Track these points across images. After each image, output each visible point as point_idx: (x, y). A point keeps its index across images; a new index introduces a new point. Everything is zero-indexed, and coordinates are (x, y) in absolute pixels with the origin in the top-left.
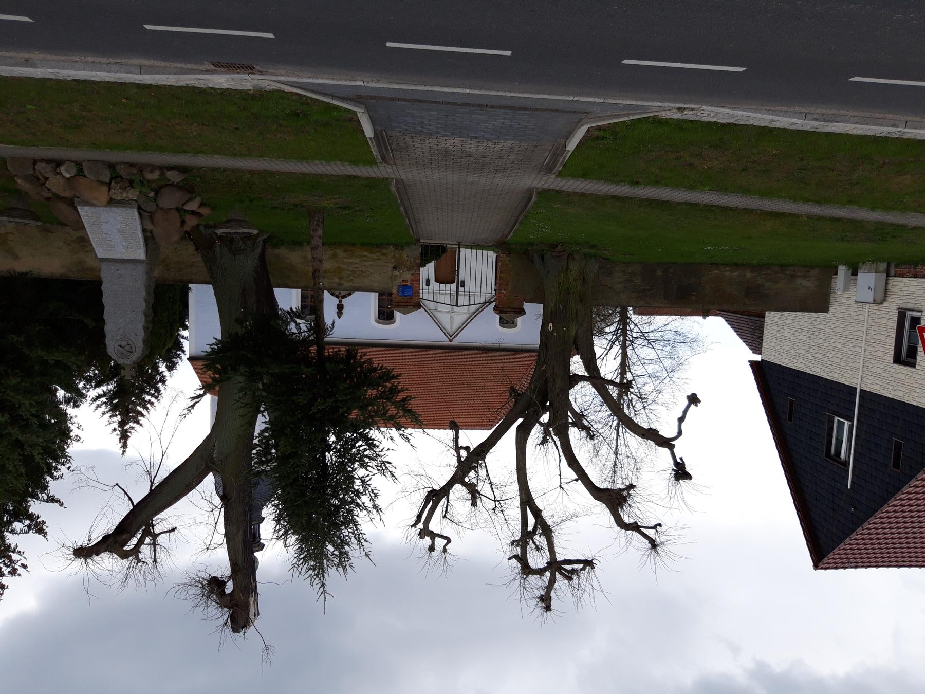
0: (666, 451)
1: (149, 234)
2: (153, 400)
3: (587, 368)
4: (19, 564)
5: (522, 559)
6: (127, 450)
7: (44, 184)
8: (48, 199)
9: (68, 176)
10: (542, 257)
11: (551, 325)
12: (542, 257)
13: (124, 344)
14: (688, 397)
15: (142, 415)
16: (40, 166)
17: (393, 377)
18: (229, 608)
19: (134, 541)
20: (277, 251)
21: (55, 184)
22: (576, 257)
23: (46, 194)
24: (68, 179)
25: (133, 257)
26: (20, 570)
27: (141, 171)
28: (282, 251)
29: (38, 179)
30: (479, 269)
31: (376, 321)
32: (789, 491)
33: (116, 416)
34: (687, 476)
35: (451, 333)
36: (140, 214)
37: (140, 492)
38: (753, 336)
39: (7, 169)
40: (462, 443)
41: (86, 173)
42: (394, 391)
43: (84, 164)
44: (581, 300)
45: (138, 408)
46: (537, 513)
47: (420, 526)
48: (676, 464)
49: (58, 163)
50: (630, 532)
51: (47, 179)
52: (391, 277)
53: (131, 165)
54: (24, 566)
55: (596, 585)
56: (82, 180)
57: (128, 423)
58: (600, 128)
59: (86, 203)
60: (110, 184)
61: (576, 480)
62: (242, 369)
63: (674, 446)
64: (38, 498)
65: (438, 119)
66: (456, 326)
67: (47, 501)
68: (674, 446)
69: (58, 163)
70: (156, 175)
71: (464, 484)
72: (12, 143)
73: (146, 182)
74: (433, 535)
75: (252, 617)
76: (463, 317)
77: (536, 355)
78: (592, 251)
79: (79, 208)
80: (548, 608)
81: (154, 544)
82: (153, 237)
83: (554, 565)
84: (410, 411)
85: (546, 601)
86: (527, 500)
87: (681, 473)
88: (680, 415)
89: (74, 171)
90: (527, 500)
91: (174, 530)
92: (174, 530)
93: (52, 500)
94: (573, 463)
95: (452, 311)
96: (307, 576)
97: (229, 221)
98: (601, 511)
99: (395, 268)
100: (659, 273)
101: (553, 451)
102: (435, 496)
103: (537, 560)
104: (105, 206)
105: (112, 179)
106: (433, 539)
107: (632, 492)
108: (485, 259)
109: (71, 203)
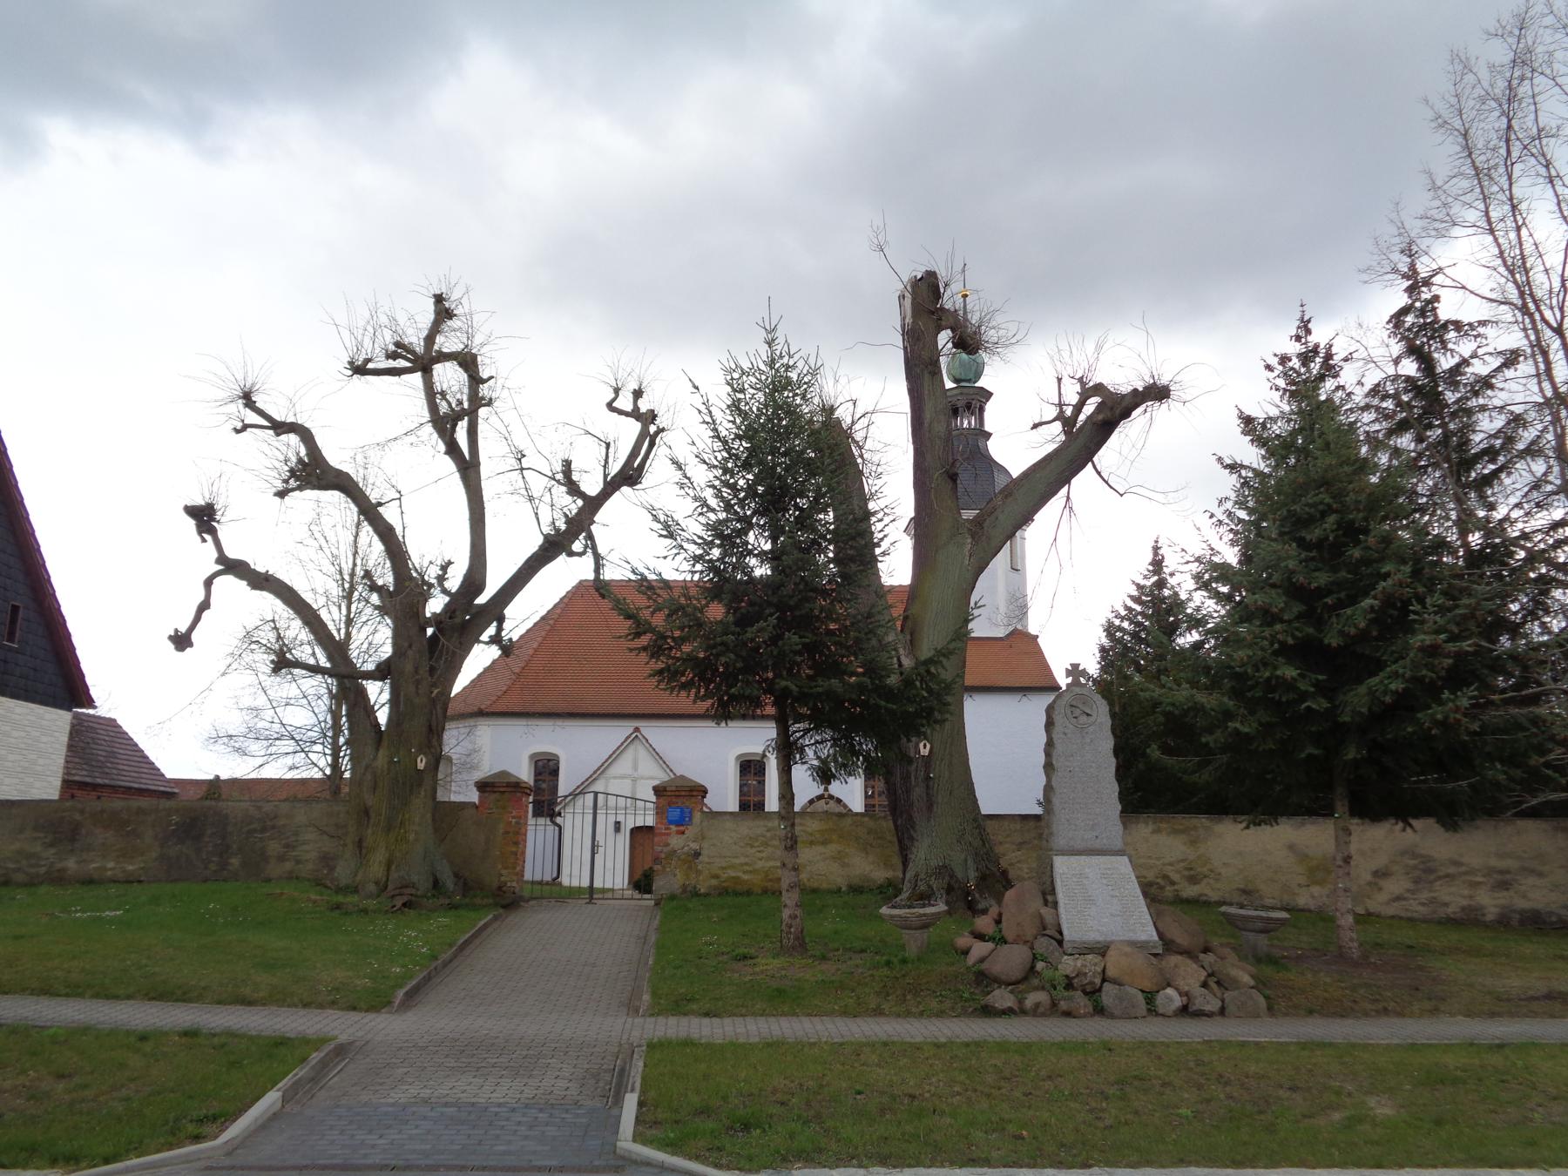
0: (232, 553)
1: (1050, 898)
2: (1117, 622)
3: (363, 693)
4: (1276, 373)
5: (475, 380)
7: (1209, 975)
8: (1206, 950)
9: (1169, 991)
10: (436, 884)
11: (421, 766)
12: (436, 884)
13: (1084, 719)
14: (191, 645)
15: (1131, 597)
16: (1214, 1005)
17: (660, 672)
18: (942, 309)
20: (890, 874)
21: (1190, 975)
22: (372, 888)
23: (1208, 959)
24: (1169, 985)
25: (1073, 859)
26: (1274, 362)
27: (1054, 1004)
28: (880, 875)
29: (1218, 983)
30: (587, 850)
32: (21, 486)
34: (192, 511)
36: (1061, 933)
37: (1084, 480)
38: (102, 757)
39: (1267, 998)
40: (589, 560)
41: (1140, 996)
42: (656, 650)
43: (1144, 1013)
44: (367, 812)
45: (1139, 608)
46: (452, 449)
47: (653, 429)
48: (213, 532)
49: (1185, 1011)
50: (290, 419)
51: (1205, 985)
53: (1068, 1014)
54: (1269, 368)
55: (346, 334)
56: (1148, 986)
57: (1154, 584)
58: (197, 1138)
59: (1140, 946)
60: (1104, 980)
61: (380, 504)
62: (893, 680)
63: (218, 561)
64: (1254, 470)
65: (498, 1137)
66: (628, 757)
67: (1242, 466)
68: (218, 561)
69: (1185, 1011)
70: (1032, 999)
71: (582, 495)
72: (1243, 1044)
73: (1048, 986)
74: (635, 414)
75: (908, 295)
76: (615, 770)
77: (449, 712)
78: (340, 899)
79: (1156, 938)
80: (439, 299)
81: (1060, 405)
82: (1044, 894)
83: (424, 363)
84: (628, 617)
85: (443, 312)
86: (469, 469)
87: (204, 517)
88: (205, 614)
89: (1160, 999)
90: (469, 469)
91: (1035, 426)
92: (1035, 426)
93: (1233, 467)
94: (386, 534)
96: (796, 357)
97: (925, 926)
98: (336, 457)
99: (697, 854)
100: (235, 862)
101: (423, 553)
102: (630, 475)
103: (449, 377)
104: (1112, 942)
105: (1100, 990)
106: (636, 408)
107: (280, 485)
108: (576, 872)
109: (1169, 946)
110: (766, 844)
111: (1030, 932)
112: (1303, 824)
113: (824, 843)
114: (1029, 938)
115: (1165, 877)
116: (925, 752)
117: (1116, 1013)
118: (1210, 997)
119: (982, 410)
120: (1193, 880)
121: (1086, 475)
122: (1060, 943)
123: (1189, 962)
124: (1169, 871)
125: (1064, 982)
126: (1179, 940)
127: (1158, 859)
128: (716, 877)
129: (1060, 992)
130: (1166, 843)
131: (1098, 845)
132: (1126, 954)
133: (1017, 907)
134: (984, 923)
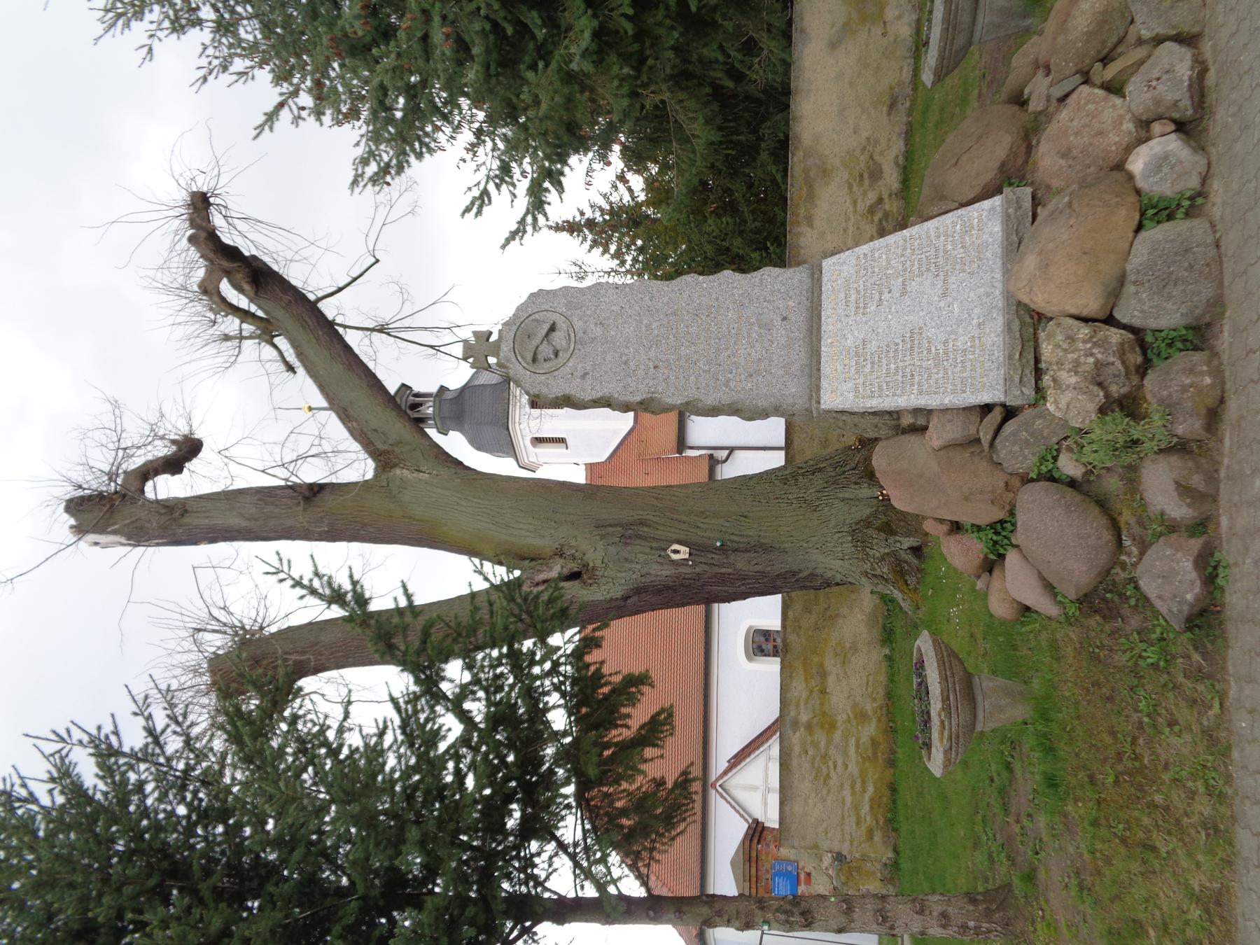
6: (552, 232)
8: (1019, 101)
9: (1138, 164)
13: (559, 338)
19: (242, 302)
24: (1119, 167)
25: (826, 368)
27: (1180, 448)
29: (1105, 60)
31: (750, 628)
33: (602, 215)
35: (727, 786)
36: (986, 409)
41: (1155, 234)
51: (1114, 88)
52: (816, 847)
53: (1213, 417)
56: (1125, 216)
60: (1110, 320)
66: (741, 795)
73: (1129, 458)
79: (997, 201)
89: (1161, 187)
95: (769, 790)
99: (839, 857)
104: (1008, 295)
110: (825, 757)
111: (985, 479)
112: (802, 31)
113: (823, 675)
114: (999, 480)
115: (872, 210)
116: (684, 552)
117: (1207, 290)
118: (1152, 70)
119: (417, 395)
120: (876, 174)
121: (329, 309)
122: (1010, 413)
123: (1052, 129)
124: (862, 206)
125: (1118, 424)
126: (1001, 153)
127: (847, 220)
128: (870, 833)
129: (1153, 428)
130: (823, 205)
131: (799, 319)
132: (1045, 267)
133: (916, 481)
134: (960, 554)
